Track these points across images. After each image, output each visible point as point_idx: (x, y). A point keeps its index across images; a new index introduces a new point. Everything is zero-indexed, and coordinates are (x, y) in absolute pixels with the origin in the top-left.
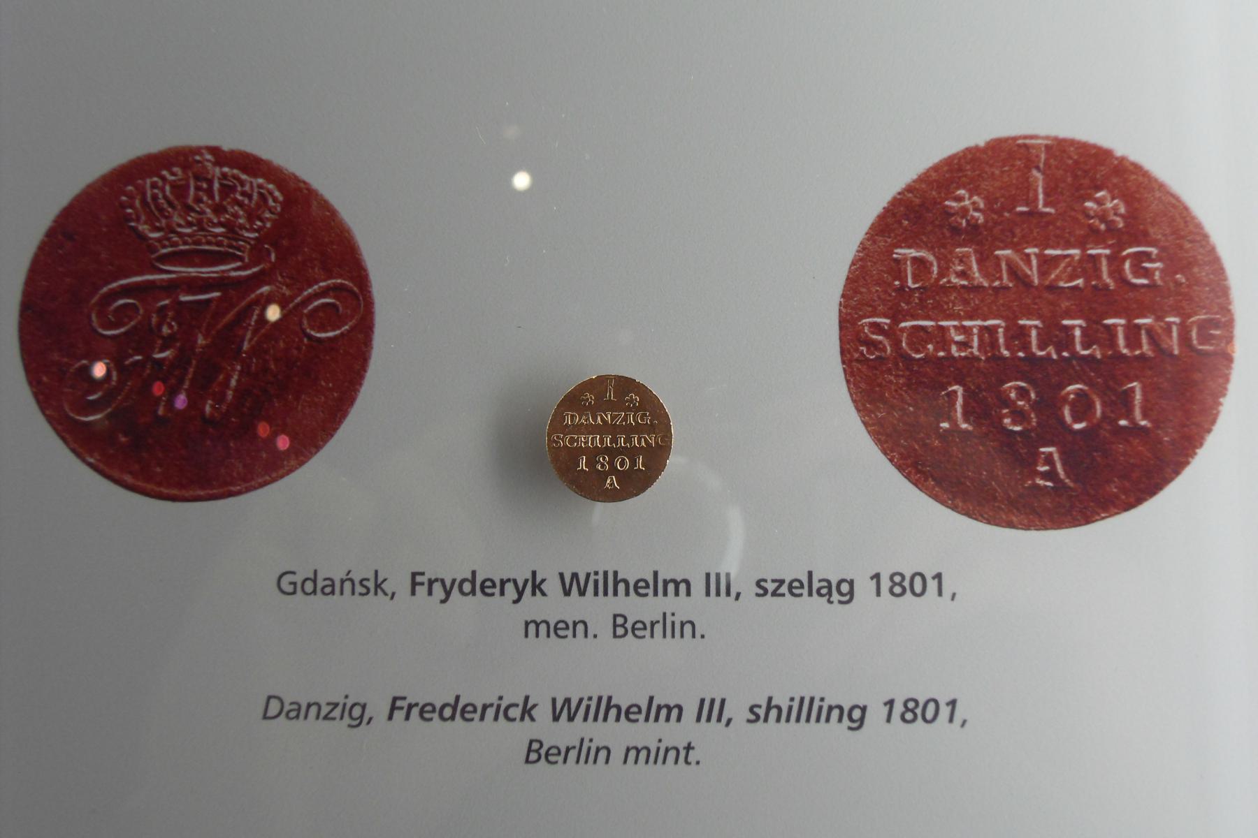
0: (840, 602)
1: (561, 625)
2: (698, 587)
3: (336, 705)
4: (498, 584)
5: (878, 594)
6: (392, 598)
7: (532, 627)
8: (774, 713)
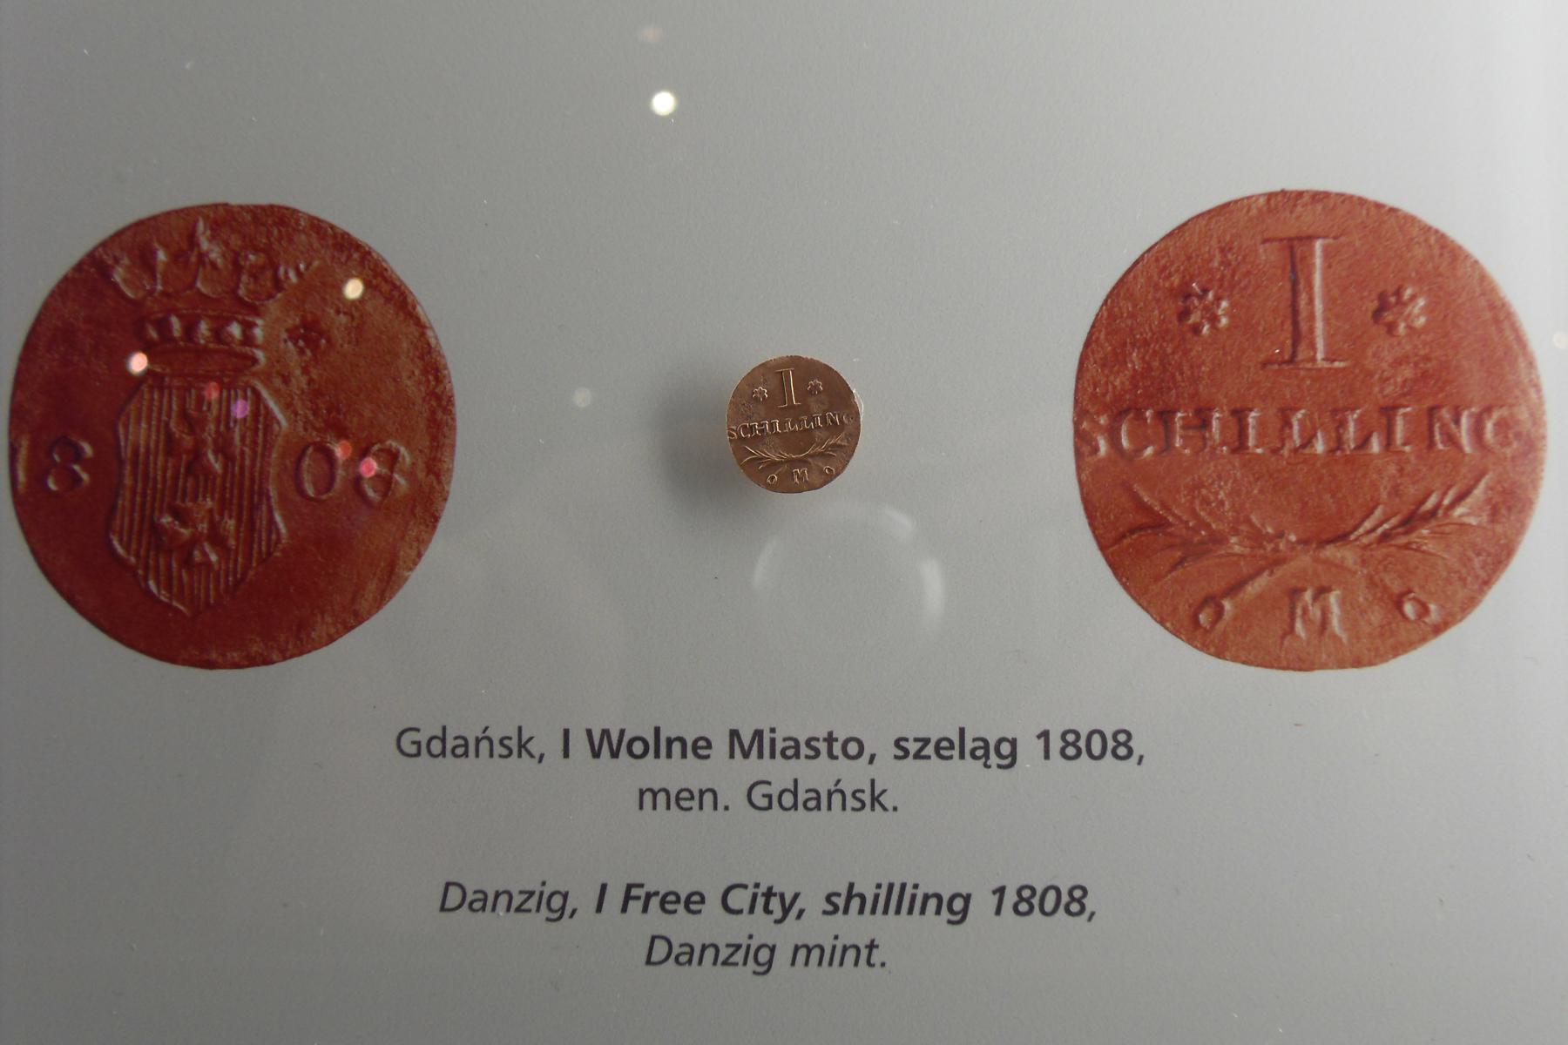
0: (1000, 766)
1: (685, 795)
3: (738, 947)
5: (1047, 756)
6: (540, 761)
7: (648, 797)
8: (855, 903)
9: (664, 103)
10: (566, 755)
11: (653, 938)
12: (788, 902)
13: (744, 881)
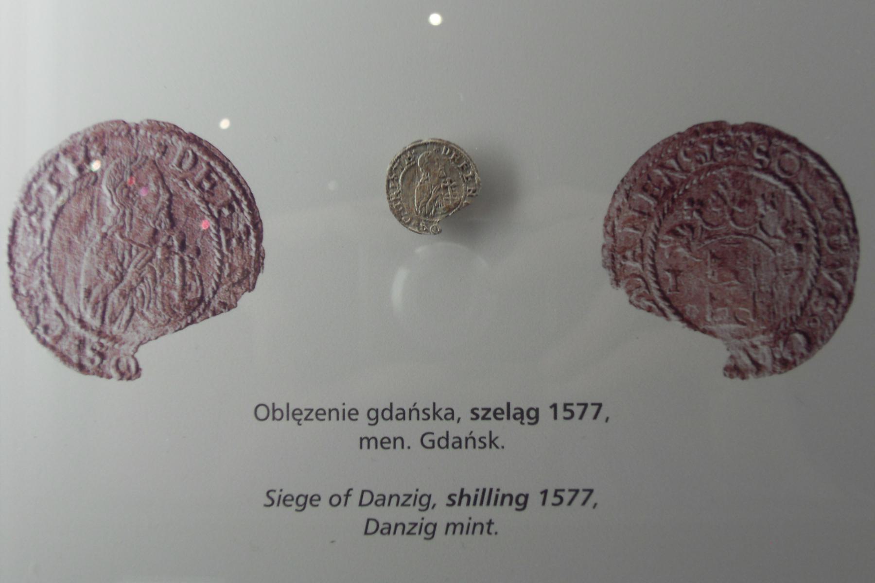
0: (529, 424)
3: (410, 496)
4: (327, 412)
6: (458, 421)
7: (365, 442)
8: (465, 499)
9: (435, 19)
11: (368, 520)
13: (274, 488)
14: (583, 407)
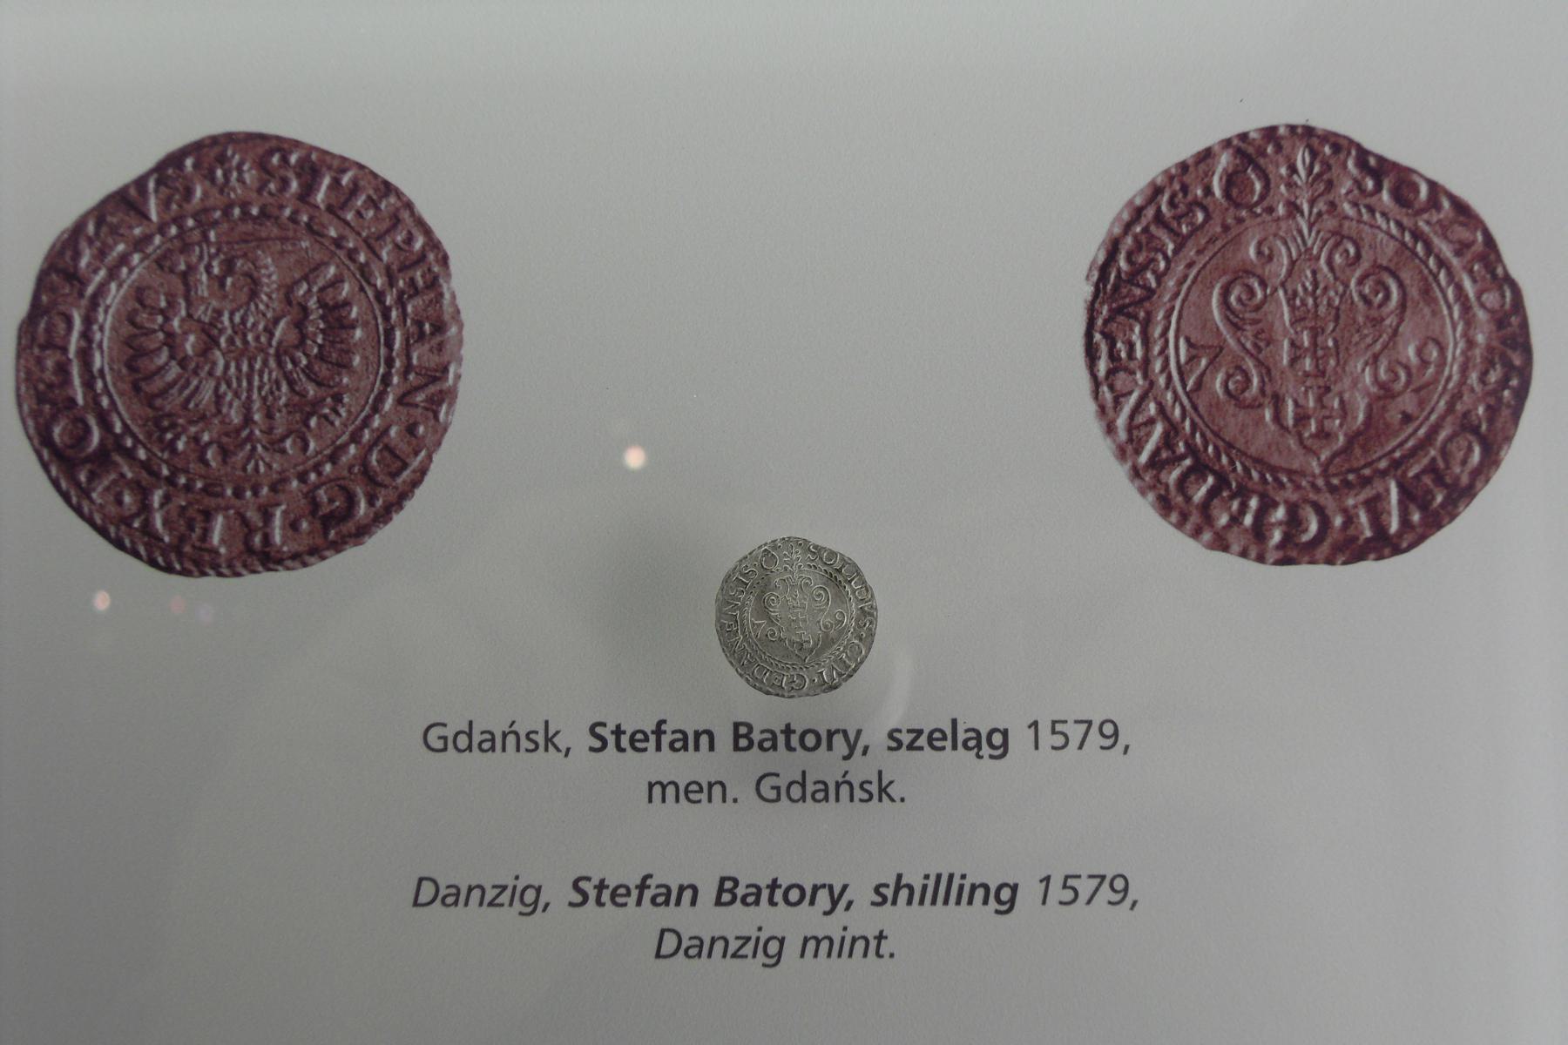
0: (991, 757)
2: (724, 739)
3: (504, 888)
6: (566, 755)
7: (657, 790)
8: (904, 893)
10: (1037, 748)
12: (837, 892)
14: (1085, 726)
